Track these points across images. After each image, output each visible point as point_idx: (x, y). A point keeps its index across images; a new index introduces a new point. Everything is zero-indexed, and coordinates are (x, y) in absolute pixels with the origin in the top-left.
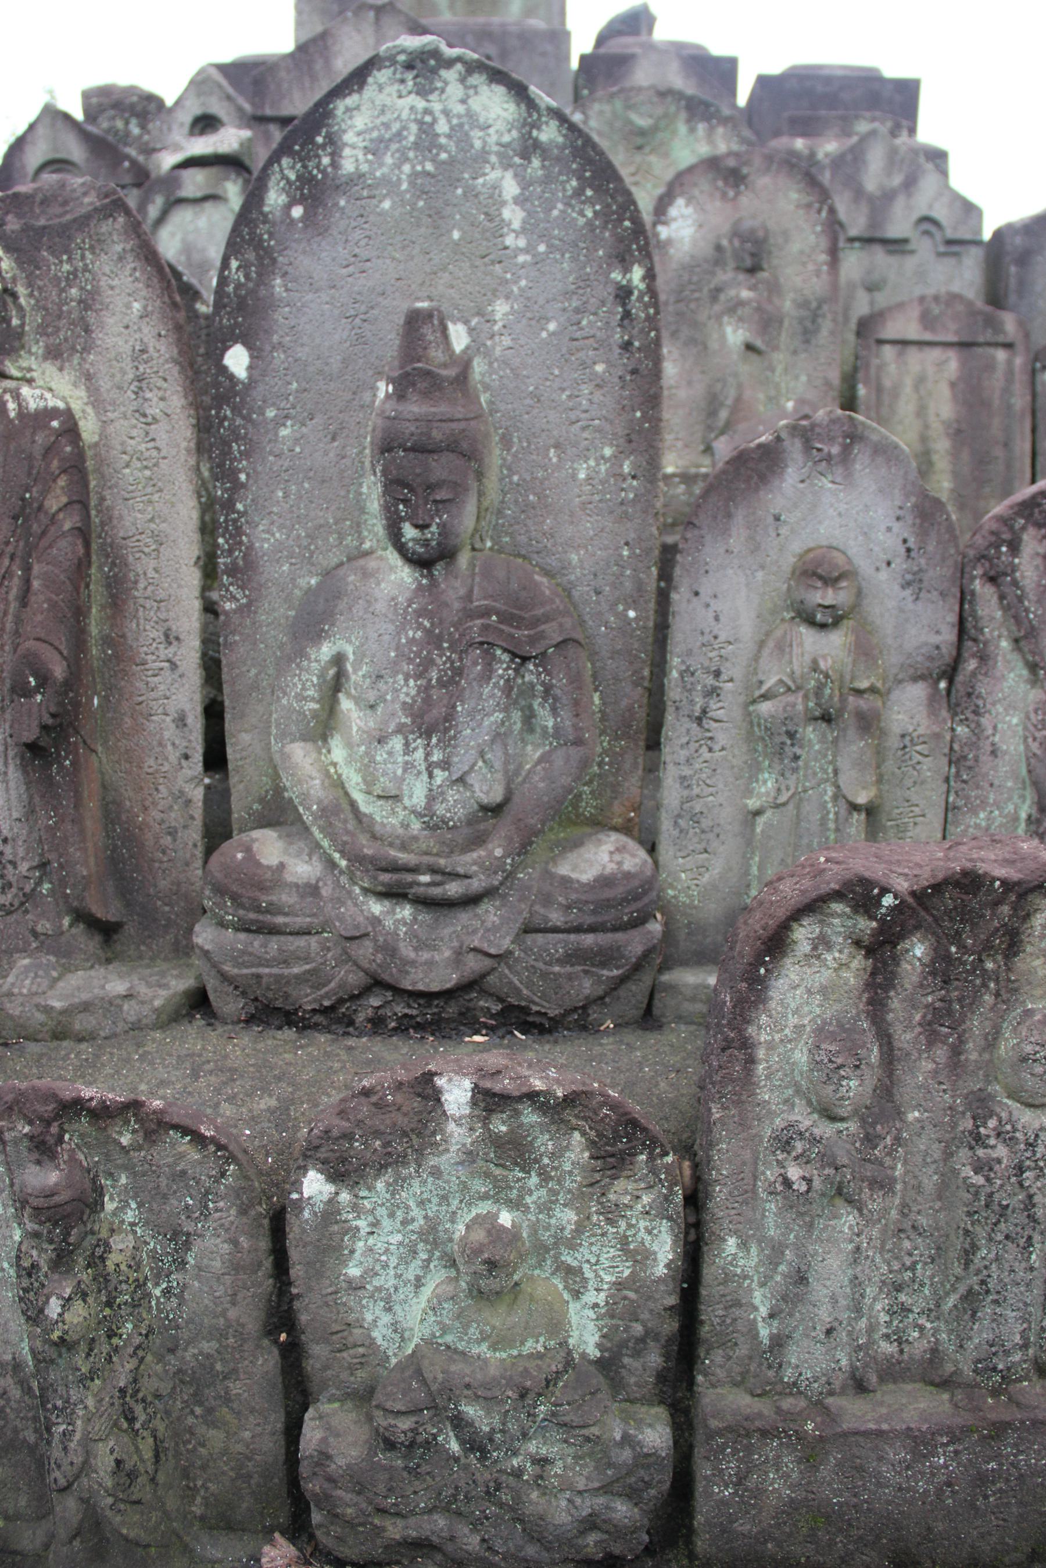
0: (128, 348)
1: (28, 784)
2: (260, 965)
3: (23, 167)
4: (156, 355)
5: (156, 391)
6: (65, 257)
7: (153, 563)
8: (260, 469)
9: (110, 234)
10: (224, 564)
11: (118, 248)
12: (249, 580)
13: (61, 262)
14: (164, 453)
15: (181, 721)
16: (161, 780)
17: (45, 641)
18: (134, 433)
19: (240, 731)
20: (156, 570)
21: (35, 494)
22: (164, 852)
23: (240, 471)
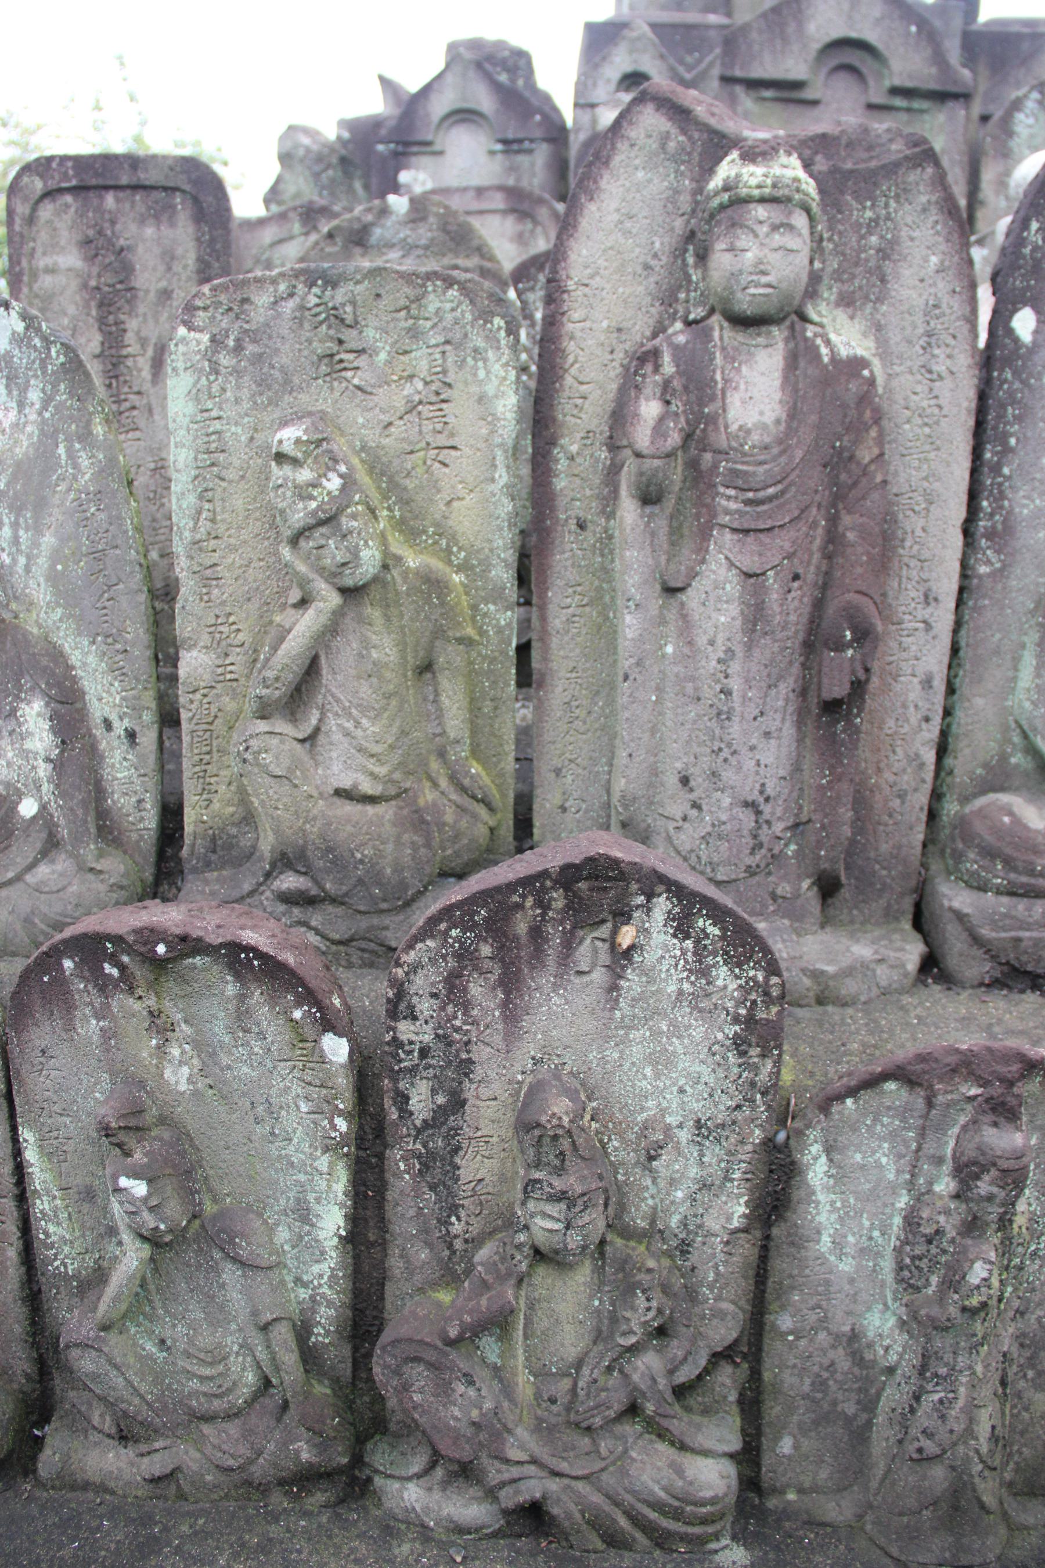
0: (920, 302)
1: (800, 741)
2: (1021, 928)
3: (428, 115)
4: (948, 311)
5: (943, 348)
6: (869, 204)
7: (921, 522)
8: (1029, 434)
9: (917, 184)
10: (985, 527)
11: (923, 199)
12: (1006, 544)
13: (864, 208)
14: (945, 412)
15: (927, 683)
16: (899, 742)
17: (866, 595)
18: (919, 388)
19: (975, 696)
20: (924, 530)
21: (845, 443)
22: (890, 816)
23: (1011, 435)
